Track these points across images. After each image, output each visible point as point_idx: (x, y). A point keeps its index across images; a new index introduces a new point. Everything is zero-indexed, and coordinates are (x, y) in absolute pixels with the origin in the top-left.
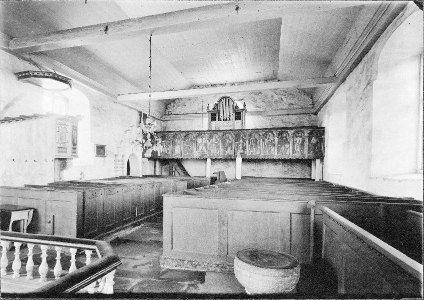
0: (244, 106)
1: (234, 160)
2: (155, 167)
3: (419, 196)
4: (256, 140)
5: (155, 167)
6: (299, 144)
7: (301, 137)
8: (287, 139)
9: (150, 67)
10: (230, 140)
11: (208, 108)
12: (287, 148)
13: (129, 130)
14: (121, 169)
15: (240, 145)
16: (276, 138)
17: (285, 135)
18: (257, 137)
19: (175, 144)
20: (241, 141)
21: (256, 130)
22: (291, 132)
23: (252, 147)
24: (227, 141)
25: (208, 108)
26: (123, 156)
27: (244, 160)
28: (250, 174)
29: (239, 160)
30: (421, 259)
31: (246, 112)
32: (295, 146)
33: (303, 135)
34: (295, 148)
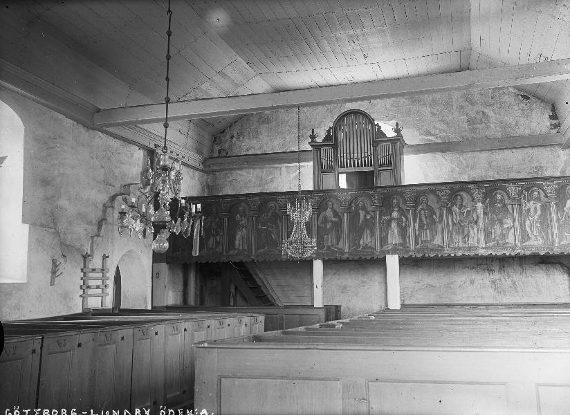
0: (397, 130)
1: (381, 263)
2: (186, 284)
3: (406, 182)
4: (432, 212)
5: (186, 284)
6: (536, 217)
7: (538, 199)
8: (505, 205)
9: (169, 33)
10: (367, 213)
11: (313, 137)
12: (509, 229)
13: (121, 194)
14: (99, 291)
15: (394, 224)
16: (480, 205)
17: (499, 196)
18: (435, 206)
19: (271, 207)
20: (395, 214)
21: (433, 188)
22: (512, 189)
23: (421, 226)
24: (362, 214)
25: (313, 137)
26: (105, 257)
27: (405, 263)
28: (421, 299)
29: (393, 261)
30: (327, 141)
31: (403, 145)
32: (528, 223)
33: (542, 194)
34: (527, 228)
